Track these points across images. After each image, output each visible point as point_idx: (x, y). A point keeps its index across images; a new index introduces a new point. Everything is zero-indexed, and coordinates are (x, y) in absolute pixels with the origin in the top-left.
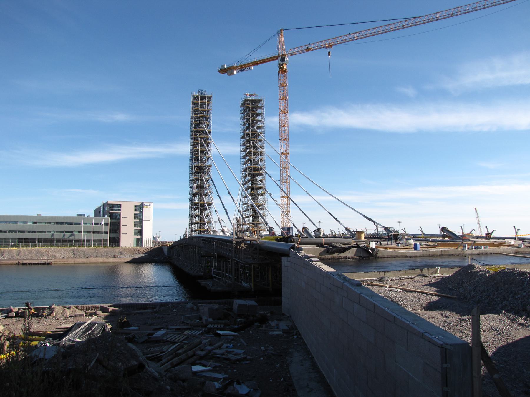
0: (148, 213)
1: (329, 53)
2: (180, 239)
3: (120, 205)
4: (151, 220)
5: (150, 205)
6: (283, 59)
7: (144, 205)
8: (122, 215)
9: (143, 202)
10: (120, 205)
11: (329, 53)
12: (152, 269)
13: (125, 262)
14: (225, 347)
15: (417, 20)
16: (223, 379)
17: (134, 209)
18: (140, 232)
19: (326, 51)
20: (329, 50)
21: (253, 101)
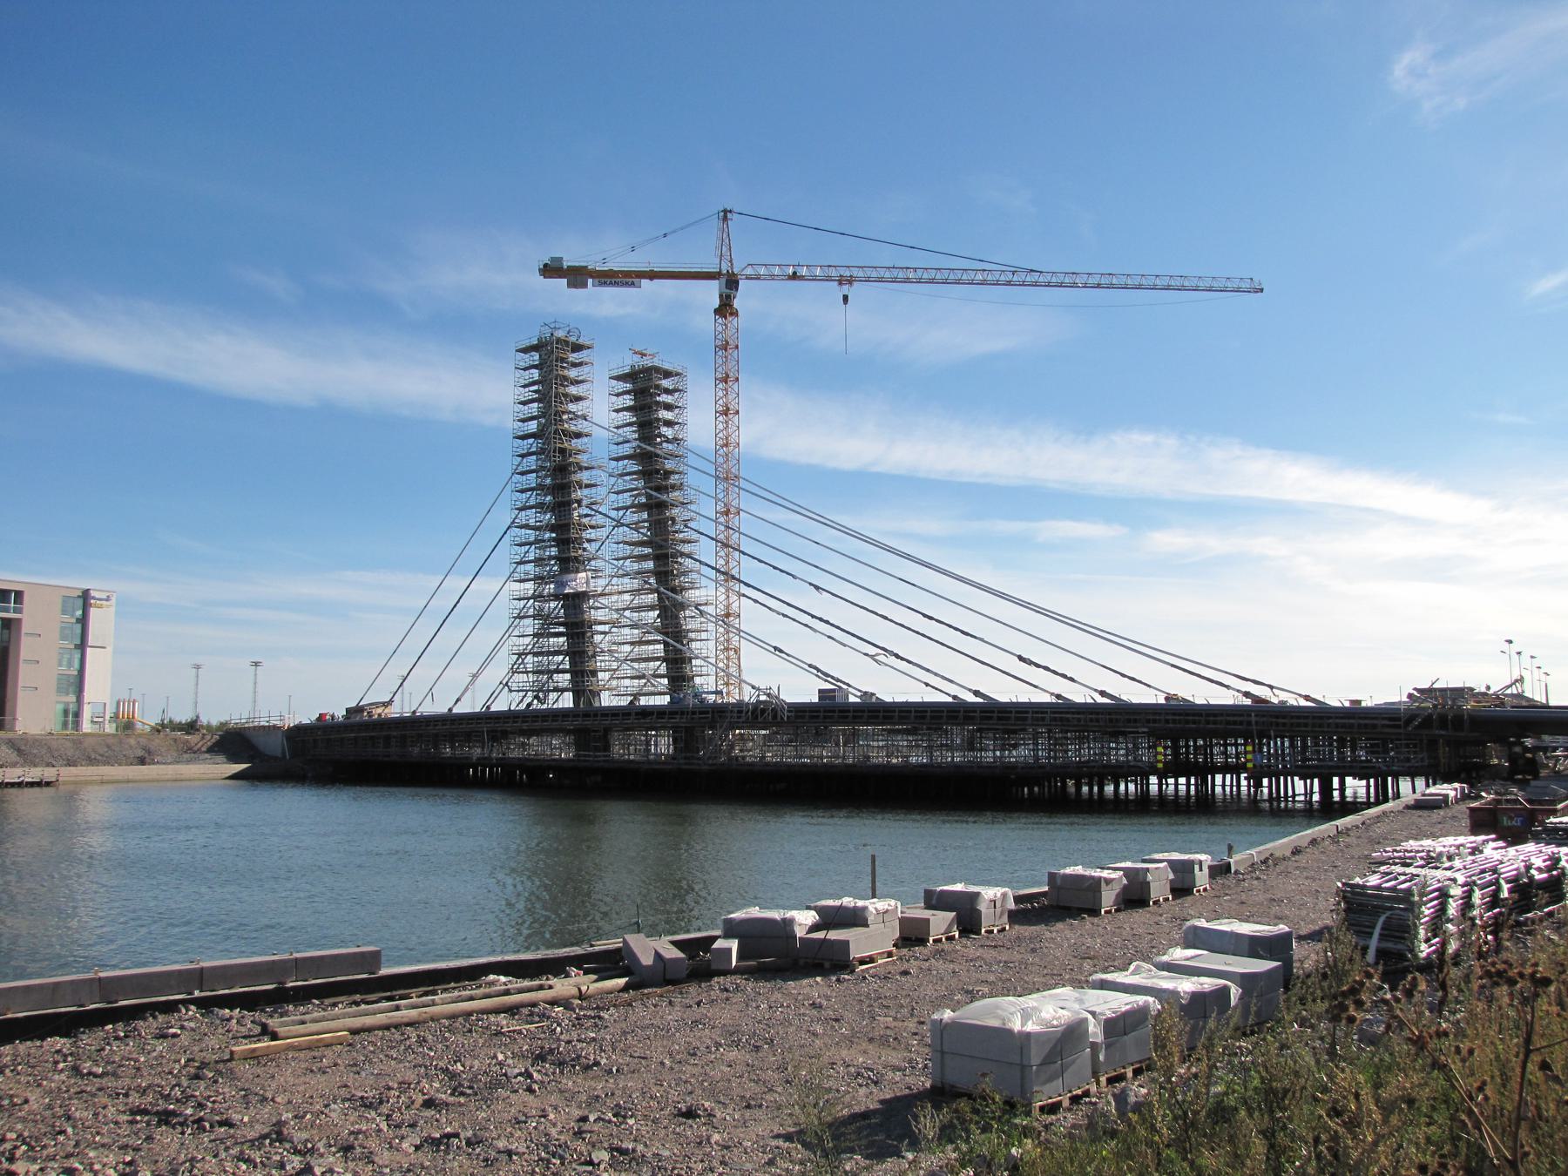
0: (99, 619)
1: (846, 298)
2: (450, 710)
3: (19, 595)
4: (110, 649)
5: (108, 599)
6: (732, 282)
7: (94, 598)
8: (25, 628)
9: (88, 590)
10: (19, 595)
11: (846, 298)
12: (345, 797)
13: (227, 775)
14: (684, 974)
15: (1034, 277)
16: (1165, 958)
17: (60, 606)
18: (78, 684)
19: (836, 291)
20: (845, 289)
21: (649, 371)
